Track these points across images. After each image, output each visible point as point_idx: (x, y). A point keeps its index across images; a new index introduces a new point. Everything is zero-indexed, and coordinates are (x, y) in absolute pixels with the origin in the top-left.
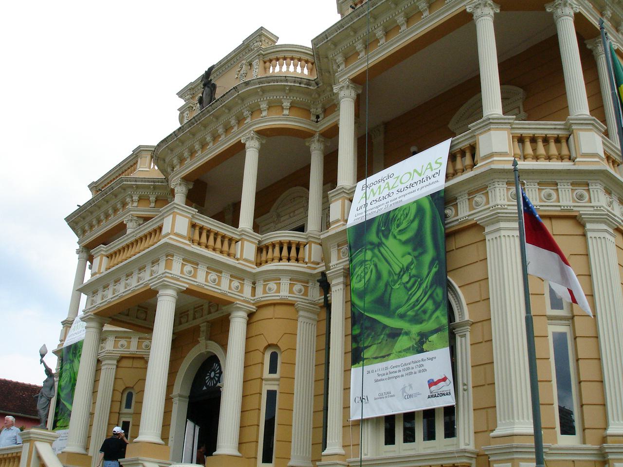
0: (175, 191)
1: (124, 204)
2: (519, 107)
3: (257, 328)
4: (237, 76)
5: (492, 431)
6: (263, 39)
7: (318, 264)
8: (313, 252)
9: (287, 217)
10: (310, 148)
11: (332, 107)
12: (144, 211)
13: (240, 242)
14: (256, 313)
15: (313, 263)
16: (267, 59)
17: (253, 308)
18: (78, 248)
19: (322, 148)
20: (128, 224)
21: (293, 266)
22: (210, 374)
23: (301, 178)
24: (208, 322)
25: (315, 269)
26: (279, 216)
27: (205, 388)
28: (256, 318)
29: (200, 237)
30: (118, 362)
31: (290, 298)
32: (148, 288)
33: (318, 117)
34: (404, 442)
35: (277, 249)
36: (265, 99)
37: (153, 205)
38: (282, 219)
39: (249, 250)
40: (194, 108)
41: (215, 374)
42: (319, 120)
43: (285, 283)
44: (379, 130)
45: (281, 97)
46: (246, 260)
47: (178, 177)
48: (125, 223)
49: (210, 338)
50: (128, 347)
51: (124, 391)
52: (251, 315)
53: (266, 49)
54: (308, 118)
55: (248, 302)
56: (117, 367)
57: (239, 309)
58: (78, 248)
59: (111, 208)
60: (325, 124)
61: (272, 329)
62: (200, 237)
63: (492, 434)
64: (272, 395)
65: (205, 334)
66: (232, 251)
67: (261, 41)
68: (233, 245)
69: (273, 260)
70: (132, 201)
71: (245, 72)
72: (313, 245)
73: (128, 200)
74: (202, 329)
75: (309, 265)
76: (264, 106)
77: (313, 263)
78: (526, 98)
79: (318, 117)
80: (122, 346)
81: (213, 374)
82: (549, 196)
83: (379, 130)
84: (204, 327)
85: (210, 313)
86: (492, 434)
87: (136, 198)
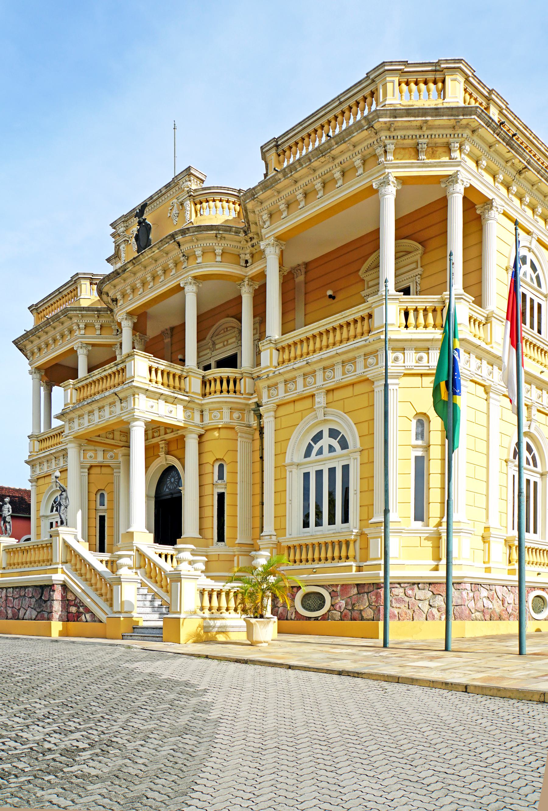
0: (123, 325)
1: (71, 331)
2: (417, 262)
3: (207, 446)
4: (169, 215)
5: (370, 519)
6: (192, 178)
7: (252, 395)
8: (245, 385)
9: (221, 345)
10: (240, 290)
11: (258, 255)
12: (93, 338)
13: (188, 379)
14: (205, 435)
15: (248, 394)
16: (197, 200)
17: (203, 432)
18: (30, 369)
19: (251, 291)
20: (78, 351)
21: (231, 398)
22: (171, 479)
23: (233, 309)
24: (165, 440)
25: (250, 399)
26: (214, 344)
27: (167, 490)
28: (204, 439)
29: (156, 376)
30: (89, 470)
31: (231, 424)
32: (119, 420)
33: (247, 262)
34: (415, 520)
35: (218, 383)
36: (199, 246)
37: (98, 332)
38: (217, 347)
39: (195, 385)
40: (130, 242)
41: (175, 479)
42: (248, 265)
43: (226, 412)
44: (300, 270)
45: (214, 244)
46: (194, 393)
47: (122, 311)
48: (75, 349)
49: (168, 453)
50: (96, 457)
51: (97, 492)
52: (200, 436)
53: (196, 190)
54: (239, 264)
55: (199, 427)
56: (89, 474)
57: (192, 432)
58: (30, 369)
59: (58, 334)
60: (253, 270)
61: (216, 448)
62: (156, 376)
63: (370, 521)
64: (221, 497)
65: (164, 450)
66: (183, 386)
67: (190, 181)
68: (182, 381)
69: (215, 392)
70: (79, 328)
71: (177, 212)
72: (247, 379)
73: (75, 327)
74: (161, 446)
75: (244, 396)
76: (198, 252)
77: (248, 394)
78: (424, 254)
79: (247, 262)
80: (91, 457)
81: (173, 480)
82: (420, 359)
83: (300, 270)
84: (162, 445)
85: (166, 433)
86: (370, 521)
87: (82, 326)
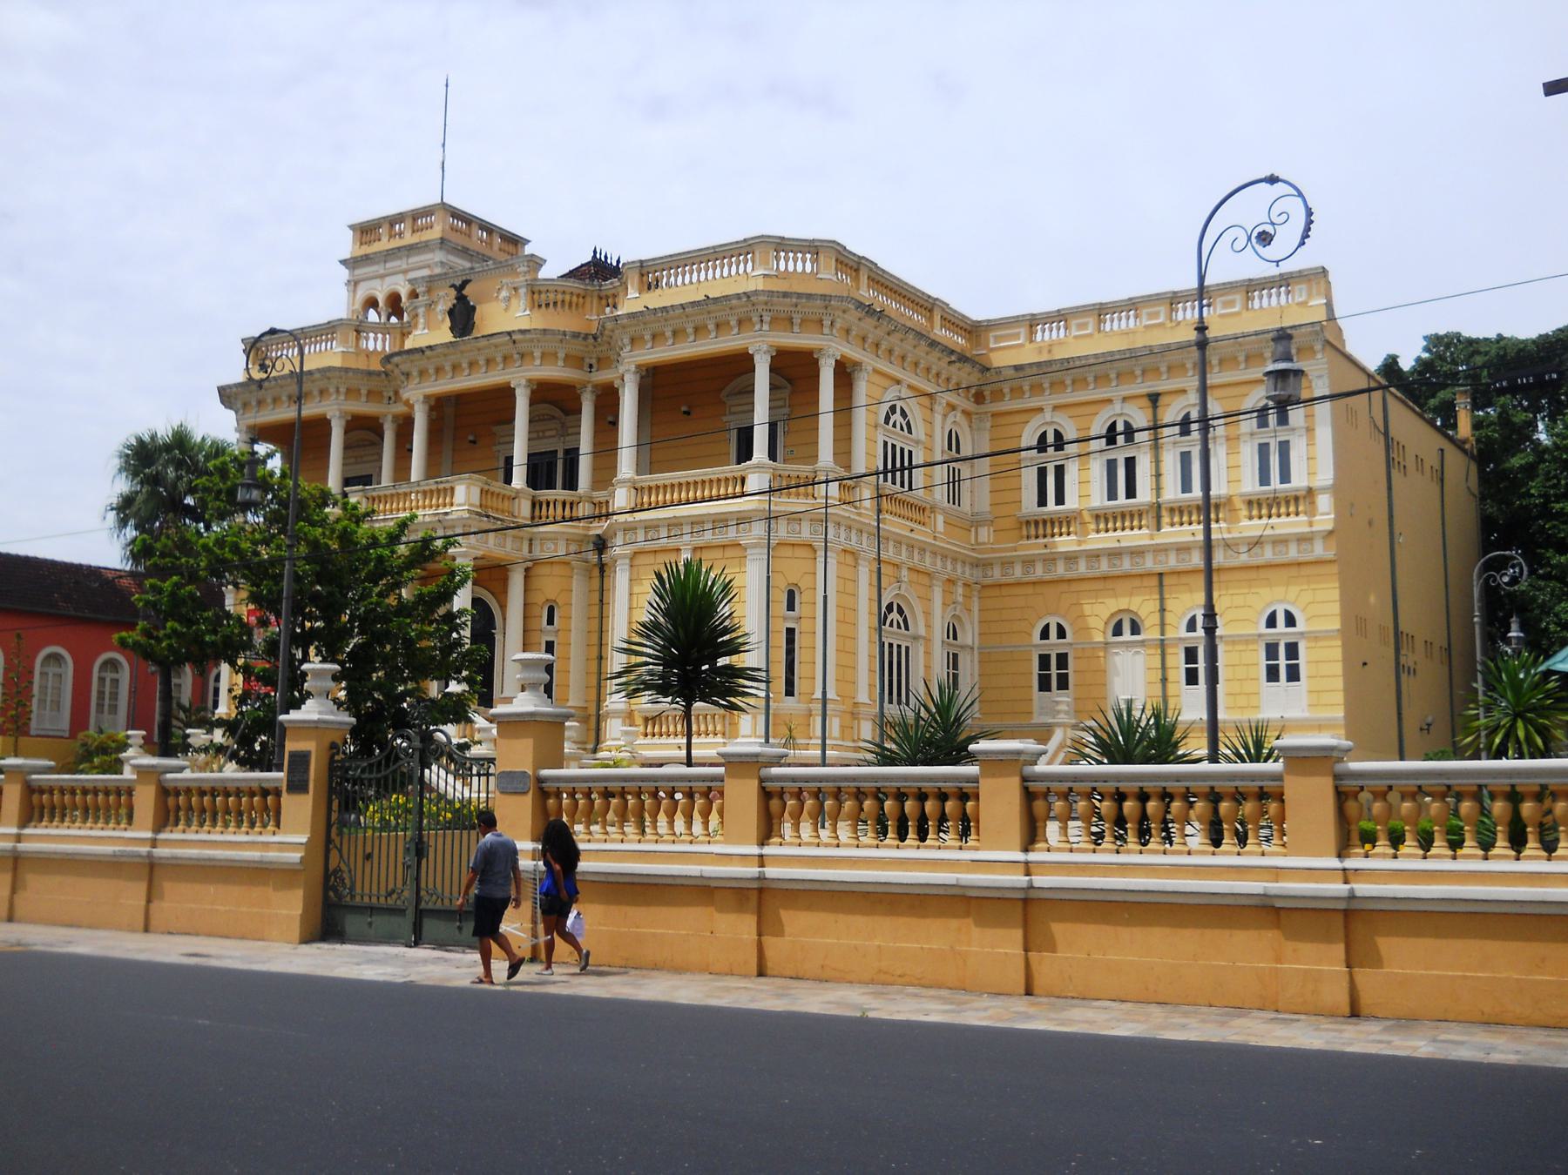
28: (532, 573)
33: (591, 366)
79: (591, 366)
